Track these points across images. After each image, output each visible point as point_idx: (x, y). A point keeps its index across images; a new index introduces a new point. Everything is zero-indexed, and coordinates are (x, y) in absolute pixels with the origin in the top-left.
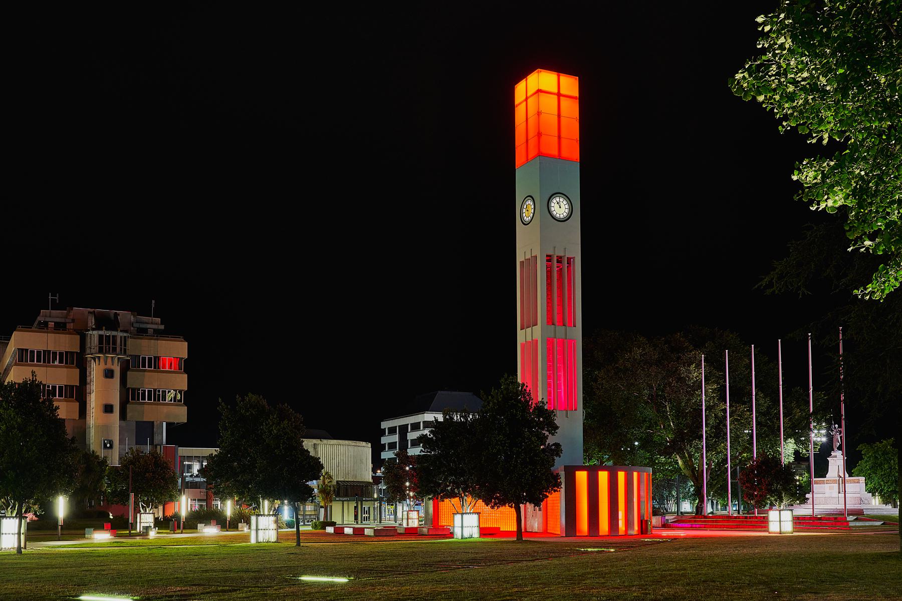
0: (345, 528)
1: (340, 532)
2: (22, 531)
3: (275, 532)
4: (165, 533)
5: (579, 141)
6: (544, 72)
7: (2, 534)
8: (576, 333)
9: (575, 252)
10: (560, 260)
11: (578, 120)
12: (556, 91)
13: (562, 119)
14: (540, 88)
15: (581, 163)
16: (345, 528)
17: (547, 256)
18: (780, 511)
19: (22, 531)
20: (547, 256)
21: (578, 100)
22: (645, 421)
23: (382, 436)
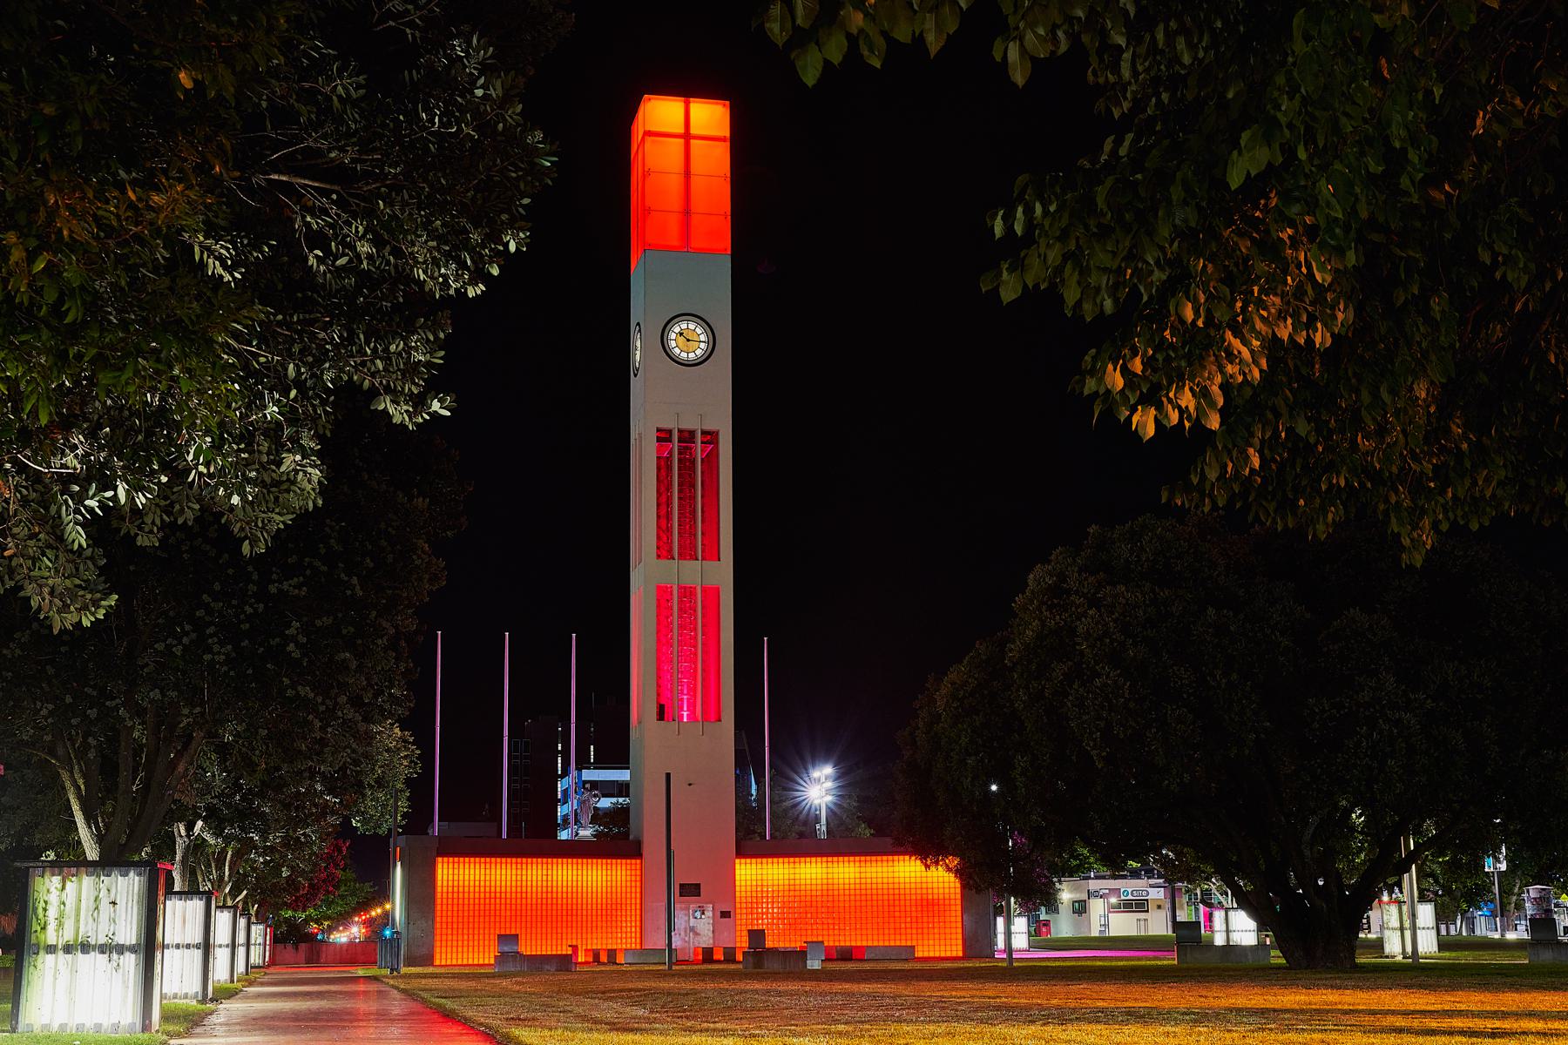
0: (1178, 919)
1: (908, 956)
2: (268, 943)
3: (1433, 933)
4: (338, 971)
5: (729, 217)
6: (655, 99)
7: (1419, 928)
8: (721, 574)
9: (722, 422)
10: (687, 437)
11: (729, 179)
12: (681, 130)
13: (693, 179)
14: (647, 129)
15: (732, 255)
16: (1178, 919)
17: (658, 430)
18: (1227, 910)
19: (268, 943)
20: (658, 430)
21: (728, 144)
22: (337, 845)
23: (1141, 439)
